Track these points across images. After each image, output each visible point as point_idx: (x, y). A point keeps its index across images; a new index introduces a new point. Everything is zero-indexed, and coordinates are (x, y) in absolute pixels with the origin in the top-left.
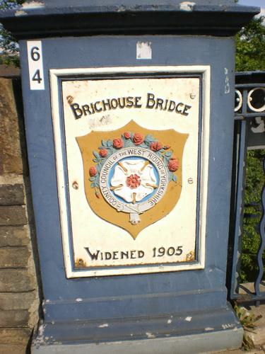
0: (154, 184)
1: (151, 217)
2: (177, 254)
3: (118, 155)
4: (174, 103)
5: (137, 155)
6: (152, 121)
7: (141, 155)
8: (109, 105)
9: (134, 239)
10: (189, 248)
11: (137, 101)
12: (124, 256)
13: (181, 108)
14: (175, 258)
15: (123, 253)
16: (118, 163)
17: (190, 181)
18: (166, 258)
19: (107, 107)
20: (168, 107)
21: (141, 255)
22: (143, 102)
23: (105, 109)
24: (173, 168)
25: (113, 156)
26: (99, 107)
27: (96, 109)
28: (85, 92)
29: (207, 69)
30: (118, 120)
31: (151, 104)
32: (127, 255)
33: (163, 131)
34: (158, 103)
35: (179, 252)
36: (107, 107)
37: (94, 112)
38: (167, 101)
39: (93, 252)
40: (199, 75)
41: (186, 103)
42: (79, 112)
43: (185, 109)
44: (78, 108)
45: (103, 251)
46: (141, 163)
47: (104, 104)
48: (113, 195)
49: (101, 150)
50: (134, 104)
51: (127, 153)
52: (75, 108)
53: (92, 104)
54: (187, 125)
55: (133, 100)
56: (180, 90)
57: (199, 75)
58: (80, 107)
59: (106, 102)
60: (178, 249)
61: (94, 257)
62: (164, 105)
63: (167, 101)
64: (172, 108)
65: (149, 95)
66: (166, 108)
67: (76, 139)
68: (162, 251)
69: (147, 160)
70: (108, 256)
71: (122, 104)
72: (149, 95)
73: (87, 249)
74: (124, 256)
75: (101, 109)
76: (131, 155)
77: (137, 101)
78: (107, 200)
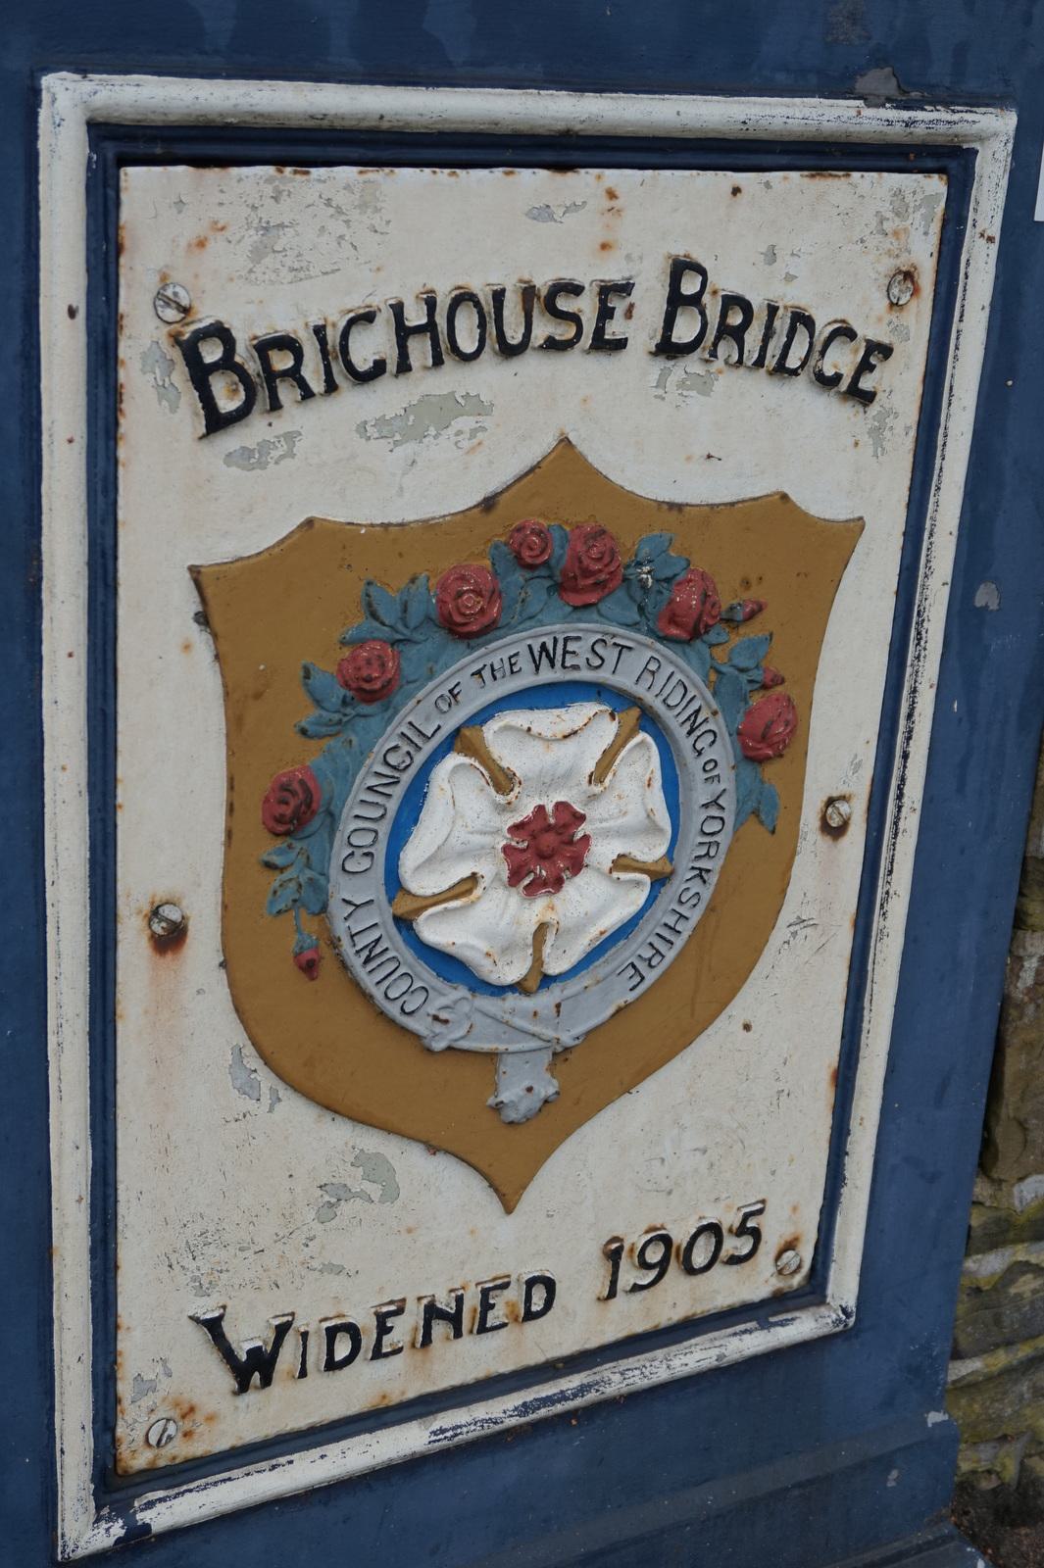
0: (652, 851)
1: (603, 1067)
2: (735, 1260)
3: (466, 679)
4: (809, 322)
5: (585, 675)
6: (675, 441)
7: (604, 676)
8: (429, 333)
9: (509, 1209)
10: (792, 1215)
11: (605, 313)
12: (440, 1329)
13: (841, 360)
14: (726, 1288)
15: (432, 1312)
16: (455, 741)
17: (170, 939)
18: (677, 1298)
19: (420, 350)
20: (771, 362)
21: (342, 1350)
22: (641, 325)
23: (404, 367)
24: (769, 740)
25: (439, 686)
26: (368, 346)
27: (455, 348)
28: (226, 248)
29: (67, 102)
30: (403, 465)
31: (685, 329)
32: (455, 1320)
33: (427, 525)
34: (724, 331)
35: (744, 1245)
36: (420, 350)
37: (331, 387)
38: (772, 310)
39: (245, 1337)
40: (952, 161)
41: (868, 330)
42: (241, 379)
43: (865, 367)
44: (227, 363)
45: (311, 1318)
46: (594, 728)
47: (403, 333)
48: (407, 955)
49: (355, 659)
50: (589, 327)
51: (524, 663)
52: (202, 355)
53: (319, 332)
54: (840, 464)
55: (586, 306)
56: (833, 245)
57: (119, 144)
58: (243, 354)
59: (415, 316)
60: (742, 1231)
61: (252, 1370)
62: (753, 337)
63: (772, 310)
64: (793, 362)
65: (680, 268)
66: (759, 363)
67: (195, 572)
68: (668, 1255)
69: (634, 701)
70: (342, 1350)
71: (514, 335)
72: (680, 268)
73: (214, 1327)
74: (440, 1329)
75: (379, 368)
76: (547, 675)
77: (605, 313)
78: (369, 982)
